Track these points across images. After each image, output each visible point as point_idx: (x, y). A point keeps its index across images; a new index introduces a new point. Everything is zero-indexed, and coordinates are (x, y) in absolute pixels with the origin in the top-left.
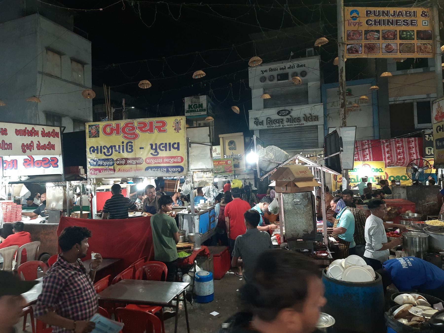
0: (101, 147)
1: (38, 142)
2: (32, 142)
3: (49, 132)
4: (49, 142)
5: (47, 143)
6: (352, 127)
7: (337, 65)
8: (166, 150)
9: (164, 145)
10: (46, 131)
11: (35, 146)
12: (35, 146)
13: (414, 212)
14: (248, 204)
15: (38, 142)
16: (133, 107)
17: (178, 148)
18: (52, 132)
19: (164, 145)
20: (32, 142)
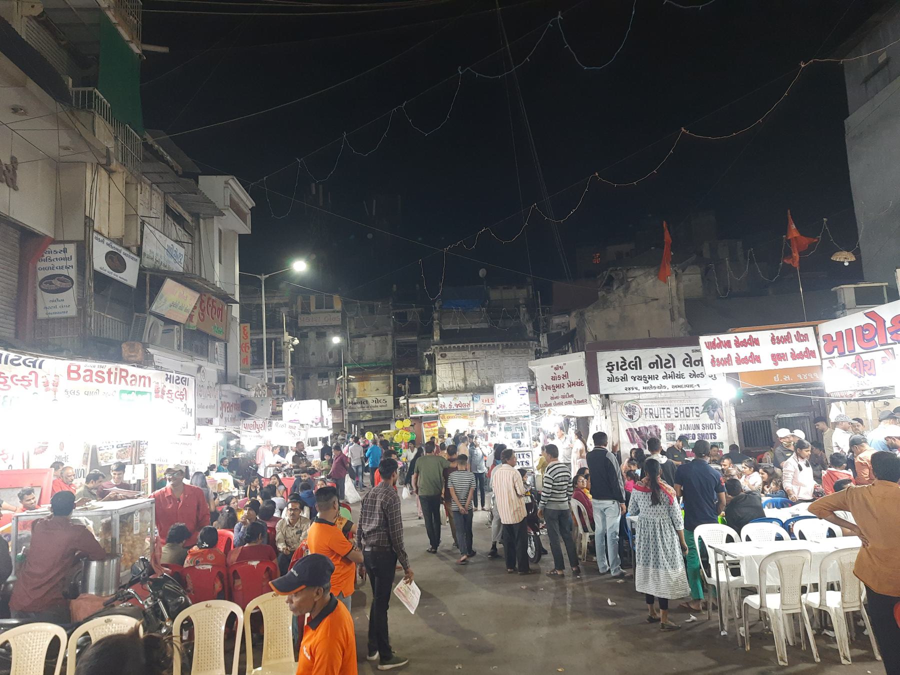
0: (115, 383)
1: (792, 349)
2: (729, 355)
3: (745, 340)
4: (807, 348)
5: (803, 350)
6: (69, 239)
7: (569, 316)
8: (637, 369)
9: (634, 363)
10: (741, 340)
11: (734, 360)
12: (734, 360)
13: (207, 544)
14: (367, 651)
15: (792, 349)
16: (255, 563)
17: (609, 364)
18: (749, 339)
19: (634, 363)
20: (729, 355)
